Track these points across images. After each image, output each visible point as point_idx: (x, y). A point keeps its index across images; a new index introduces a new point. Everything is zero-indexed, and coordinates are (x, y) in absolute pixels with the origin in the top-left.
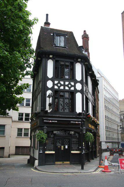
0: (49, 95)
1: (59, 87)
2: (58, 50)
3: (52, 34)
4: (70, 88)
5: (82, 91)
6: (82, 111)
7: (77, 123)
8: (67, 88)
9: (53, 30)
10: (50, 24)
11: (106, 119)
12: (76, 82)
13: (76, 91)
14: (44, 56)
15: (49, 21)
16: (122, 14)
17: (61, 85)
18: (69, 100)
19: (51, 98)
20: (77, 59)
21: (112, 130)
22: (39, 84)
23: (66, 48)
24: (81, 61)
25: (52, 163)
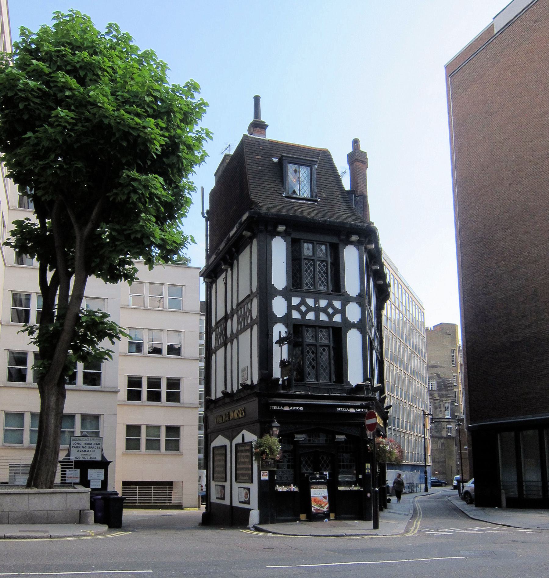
2: (296, 208)
5: (361, 326)
6: (364, 381)
8: (323, 317)
9: (275, 146)
10: (267, 126)
12: (346, 300)
13: (347, 325)
19: (285, 348)
21: (398, 427)
23: (316, 201)
25: (289, 518)
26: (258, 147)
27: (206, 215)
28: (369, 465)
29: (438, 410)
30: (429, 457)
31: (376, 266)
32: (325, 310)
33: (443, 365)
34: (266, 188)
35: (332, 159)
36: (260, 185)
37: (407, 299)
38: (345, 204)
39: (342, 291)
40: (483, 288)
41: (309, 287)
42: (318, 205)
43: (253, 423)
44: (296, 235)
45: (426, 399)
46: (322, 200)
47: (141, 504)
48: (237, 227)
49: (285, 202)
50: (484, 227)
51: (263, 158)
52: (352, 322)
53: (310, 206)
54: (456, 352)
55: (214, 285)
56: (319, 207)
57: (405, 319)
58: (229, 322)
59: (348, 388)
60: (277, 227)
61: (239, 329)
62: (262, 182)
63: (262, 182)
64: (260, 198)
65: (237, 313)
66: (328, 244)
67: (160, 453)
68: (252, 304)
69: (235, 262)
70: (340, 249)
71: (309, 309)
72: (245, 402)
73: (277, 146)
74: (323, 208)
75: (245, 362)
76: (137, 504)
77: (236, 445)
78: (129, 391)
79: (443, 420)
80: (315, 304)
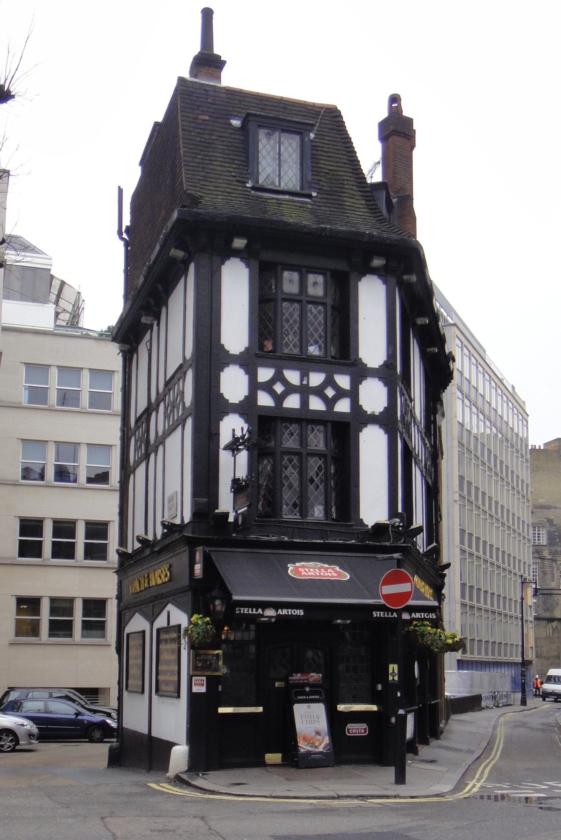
3: (236, 123)
4: (330, 403)
10: (224, 63)
11: (466, 547)
15: (217, 50)
18: (325, 463)
19: (243, 456)
23: (309, 196)
26: (204, 100)
27: (125, 236)
28: (396, 667)
29: (549, 577)
30: (530, 650)
31: (422, 319)
32: (319, 392)
34: (215, 172)
35: (344, 122)
36: (205, 166)
39: (353, 357)
41: (291, 349)
43: (182, 591)
44: (268, 256)
46: (320, 196)
48: (160, 243)
51: (213, 119)
52: (369, 413)
53: (296, 204)
55: (135, 355)
56: (315, 207)
58: (154, 415)
59: (359, 529)
60: (231, 241)
61: (167, 428)
62: (210, 162)
63: (210, 162)
64: (202, 190)
65: (164, 400)
66: (329, 274)
67: (39, 642)
68: (184, 381)
69: (164, 310)
70: (352, 283)
71: (290, 389)
72: (172, 555)
73: (242, 99)
74: (322, 208)
75: (173, 486)
77: (158, 631)
78: (21, 543)
79: (556, 592)
80: (302, 380)
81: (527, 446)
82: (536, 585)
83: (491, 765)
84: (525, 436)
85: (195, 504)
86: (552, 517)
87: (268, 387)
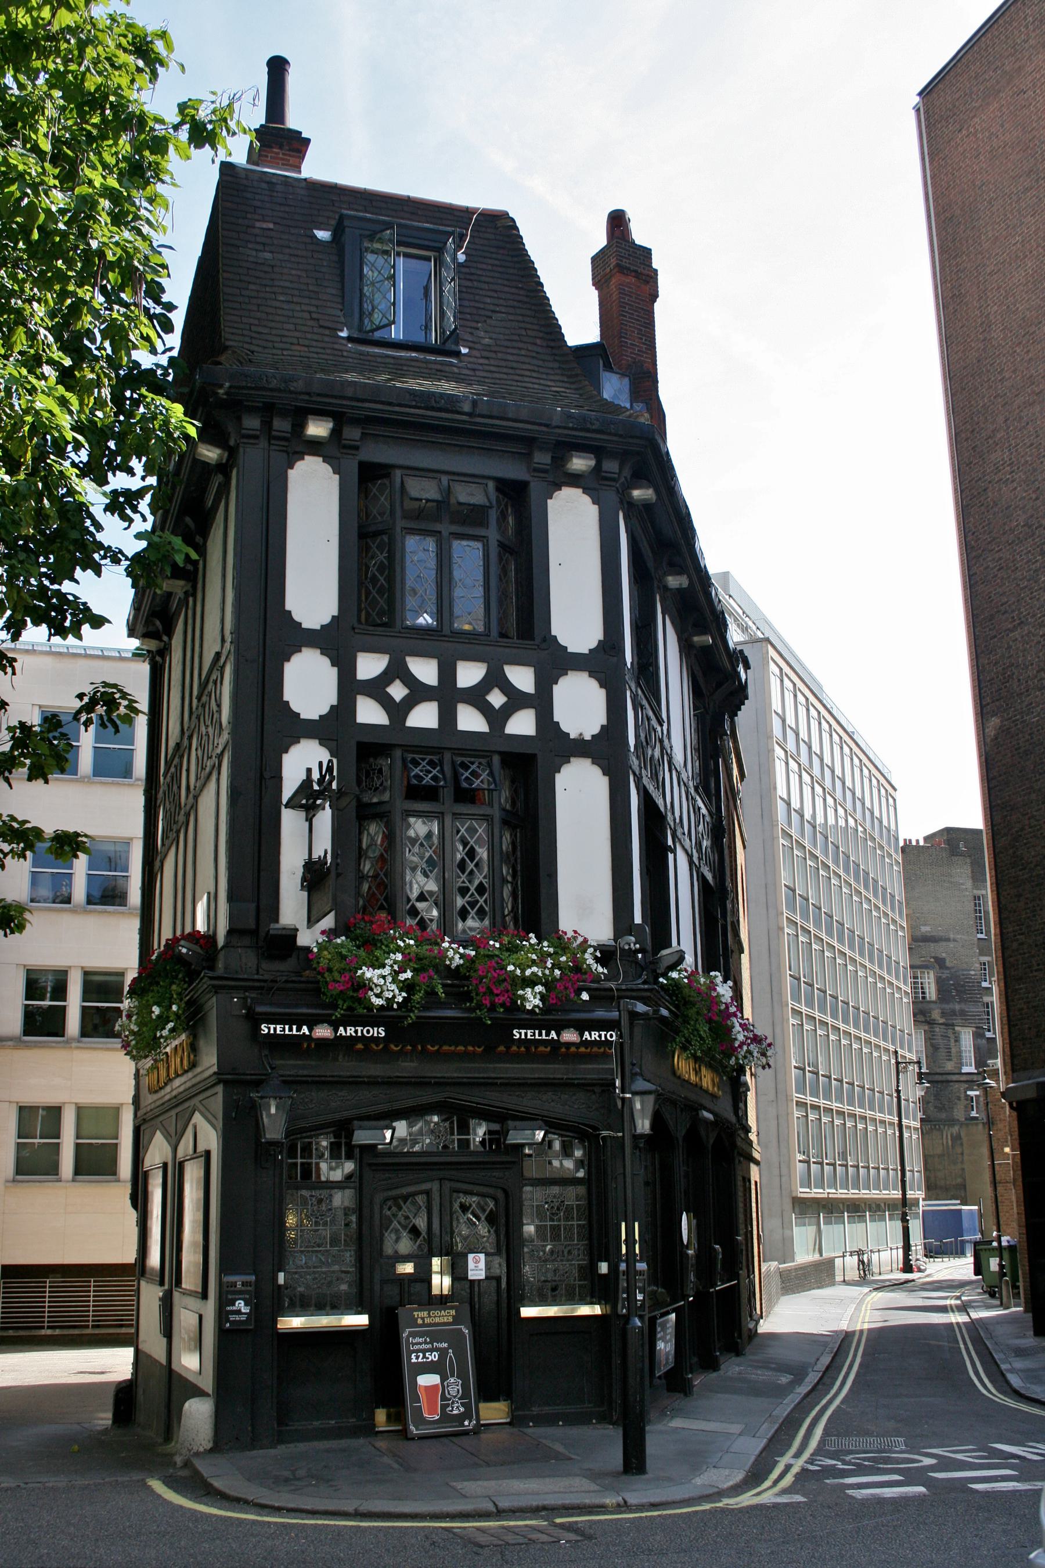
0: (307, 782)
1: (398, 711)
4: (497, 718)
7: (568, 1045)
10: (308, 141)
14: (252, 423)
15: (293, 120)
16: (925, 93)
17: (419, 693)
19: (325, 818)
20: (560, 460)
22: (203, 686)
23: (457, 354)
24: (597, 469)
29: (942, 1053)
33: (952, 936)
37: (884, 800)
38: (556, 365)
40: (1038, 672)
42: (460, 365)
45: (903, 1019)
47: (58, 1332)
49: (345, 354)
50: (1034, 496)
54: (986, 903)
57: (851, 822)
76: (43, 1332)
81: (897, 839)
82: (920, 1068)
83: (828, 1413)
84: (893, 827)
85: (232, 917)
86: (944, 955)
87: (376, 689)
